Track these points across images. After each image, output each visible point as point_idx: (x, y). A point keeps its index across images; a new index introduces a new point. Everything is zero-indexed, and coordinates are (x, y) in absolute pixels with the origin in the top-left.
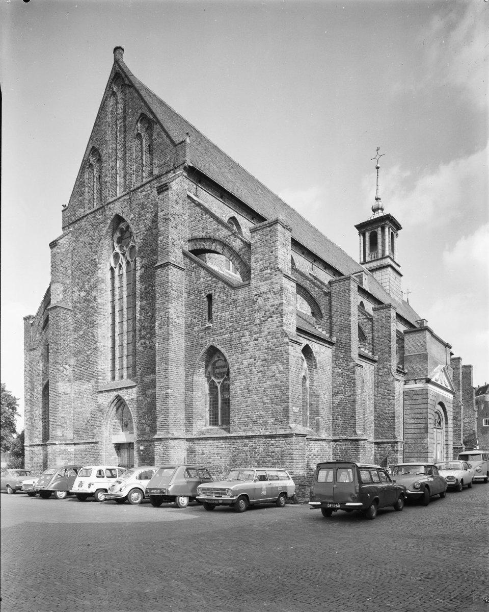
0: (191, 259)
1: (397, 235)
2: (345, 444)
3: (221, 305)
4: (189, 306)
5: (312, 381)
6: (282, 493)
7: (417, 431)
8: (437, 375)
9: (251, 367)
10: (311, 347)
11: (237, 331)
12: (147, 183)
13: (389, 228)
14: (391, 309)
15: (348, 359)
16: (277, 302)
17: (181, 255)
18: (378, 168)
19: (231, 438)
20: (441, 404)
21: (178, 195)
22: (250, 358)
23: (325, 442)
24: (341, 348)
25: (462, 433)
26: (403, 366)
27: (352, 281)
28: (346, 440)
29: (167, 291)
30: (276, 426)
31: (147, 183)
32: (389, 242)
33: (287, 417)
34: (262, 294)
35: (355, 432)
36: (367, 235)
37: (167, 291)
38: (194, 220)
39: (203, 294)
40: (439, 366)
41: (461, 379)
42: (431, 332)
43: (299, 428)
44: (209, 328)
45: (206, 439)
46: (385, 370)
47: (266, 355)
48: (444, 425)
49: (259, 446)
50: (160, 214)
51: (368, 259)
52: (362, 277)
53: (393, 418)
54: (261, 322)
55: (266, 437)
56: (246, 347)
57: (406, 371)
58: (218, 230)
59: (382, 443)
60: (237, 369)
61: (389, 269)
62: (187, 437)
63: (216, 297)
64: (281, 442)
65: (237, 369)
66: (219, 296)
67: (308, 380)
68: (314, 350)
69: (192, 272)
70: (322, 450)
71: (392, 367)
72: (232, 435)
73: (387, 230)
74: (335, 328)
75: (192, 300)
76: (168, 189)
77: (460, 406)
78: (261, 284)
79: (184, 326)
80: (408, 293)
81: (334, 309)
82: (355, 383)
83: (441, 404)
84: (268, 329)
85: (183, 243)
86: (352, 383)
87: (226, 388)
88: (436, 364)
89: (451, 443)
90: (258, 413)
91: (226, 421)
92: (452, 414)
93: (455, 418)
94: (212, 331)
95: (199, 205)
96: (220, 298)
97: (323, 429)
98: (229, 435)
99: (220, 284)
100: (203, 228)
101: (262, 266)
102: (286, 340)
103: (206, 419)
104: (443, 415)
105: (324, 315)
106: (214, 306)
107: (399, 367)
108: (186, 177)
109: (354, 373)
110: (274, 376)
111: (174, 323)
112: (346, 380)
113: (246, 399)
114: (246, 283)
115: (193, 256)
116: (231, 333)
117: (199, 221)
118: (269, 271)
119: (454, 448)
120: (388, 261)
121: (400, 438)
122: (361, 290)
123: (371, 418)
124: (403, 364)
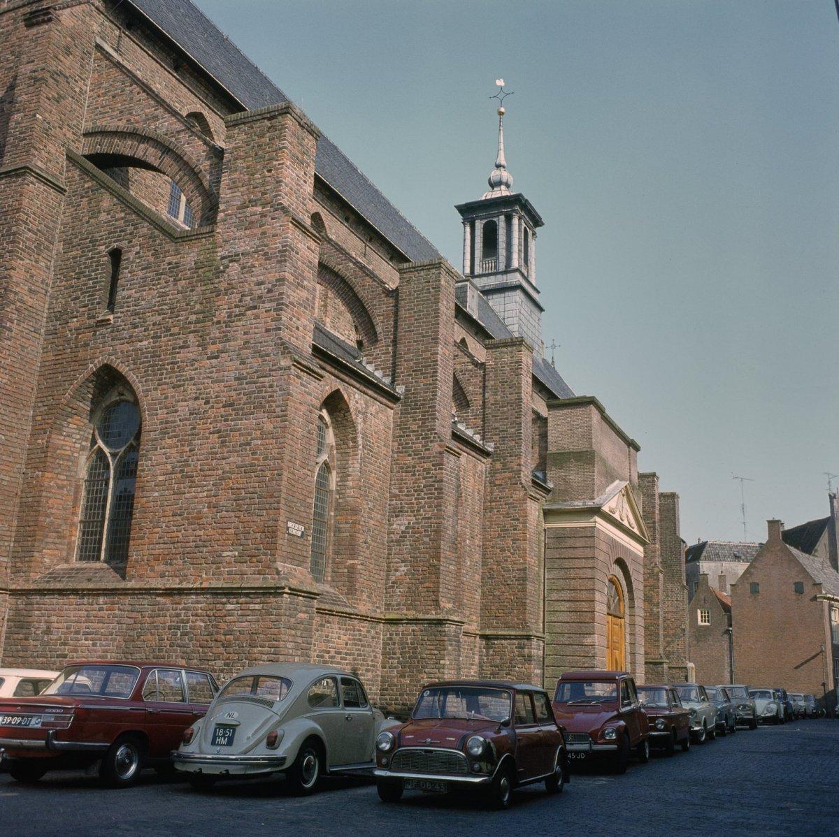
0: (85, 171)
1: (534, 234)
2: (413, 631)
3: (140, 274)
4: (65, 270)
5: (344, 477)
6: (124, 733)
7: (574, 617)
8: (614, 500)
9: (195, 418)
10: (346, 396)
11: (171, 335)
12: (9, 11)
13: (520, 219)
14: (523, 348)
15: (427, 433)
16: (272, 277)
17: (63, 160)
18: (501, 114)
19: (125, 592)
20: (620, 562)
21: (73, 39)
22: (196, 399)
23: (366, 624)
24: (415, 410)
25: (661, 632)
26: (545, 476)
27: (443, 273)
28: (416, 621)
29: (14, 229)
30: (244, 567)
31: (9, 11)
32: (520, 244)
33: (272, 546)
34: (238, 255)
35: (436, 603)
36: (479, 225)
37: (14, 229)
38: (105, 94)
39: (102, 248)
40: (617, 482)
41: (657, 518)
42: (601, 410)
43: (299, 576)
44: (104, 323)
45: (61, 592)
46: (507, 475)
47: (233, 393)
48: (627, 611)
49: (196, 615)
50: (26, 69)
51: (478, 271)
52: (466, 292)
53: (523, 580)
54: (229, 316)
55: (215, 592)
56: (188, 373)
57: (550, 485)
58: (156, 118)
59: (497, 637)
60: (161, 423)
61: (519, 292)
62: (14, 587)
63: (131, 256)
64: (252, 606)
65: (161, 423)
66: (138, 253)
67: (334, 473)
68: (352, 405)
69: (82, 197)
70: (357, 641)
71: (523, 469)
72: (131, 584)
73: (515, 221)
74: (403, 367)
75: (74, 258)
76: (50, 20)
77: (658, 575)
78: (238, 234)
79: (45, 315)
80: (553, 347)
81: (403, 326)
82: (441, 489)
83: (620, 562)
84: (245, 334)
85: (69, 135)
86: (436, 489)
87: (128, 470)
88: (611, 477)
89: (641, 650)
90: (201, 533)
91: (119, 555)
92: (641, 587)
93: (648, 599)
94: (112, 332)
95: (118, 65)
96: (140, 258)
97: (362, 591)
98: (122, 585)
99: (145, 229)
100: (121, 112)
101: (245, 197)
102: (284, 362)
103: (69, 543)
104: (625, 589)
105: (381, 337)
106: (125, 274)
107: (536, 476)
108: (97, 8)
109: (440, 465)
110: (249, 444)
111: (18, 304)
112: (422, 486)
113: (175, 497)
114: (207, 229)
115: (90, 165)
116: (156, 337)
117: (114, 97)
118: (259, 209)
119: (646, 663)
120: (516, 278)
121: (536, 628)
122: (462, 315)
123: (473, 578)
124: (544, 471)
